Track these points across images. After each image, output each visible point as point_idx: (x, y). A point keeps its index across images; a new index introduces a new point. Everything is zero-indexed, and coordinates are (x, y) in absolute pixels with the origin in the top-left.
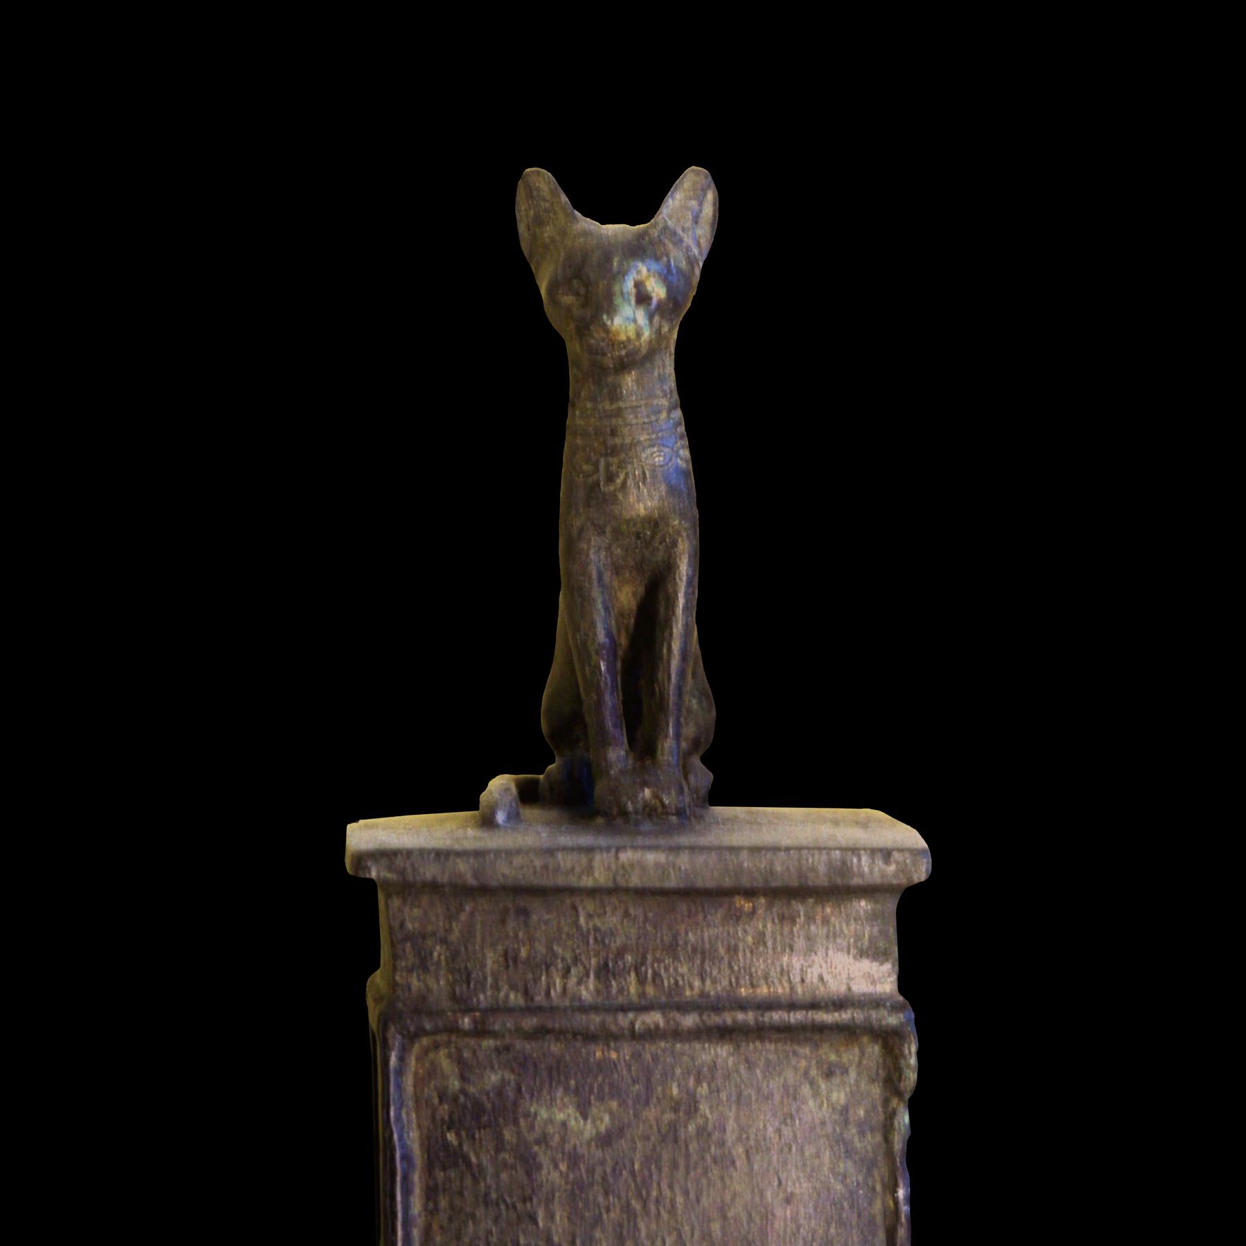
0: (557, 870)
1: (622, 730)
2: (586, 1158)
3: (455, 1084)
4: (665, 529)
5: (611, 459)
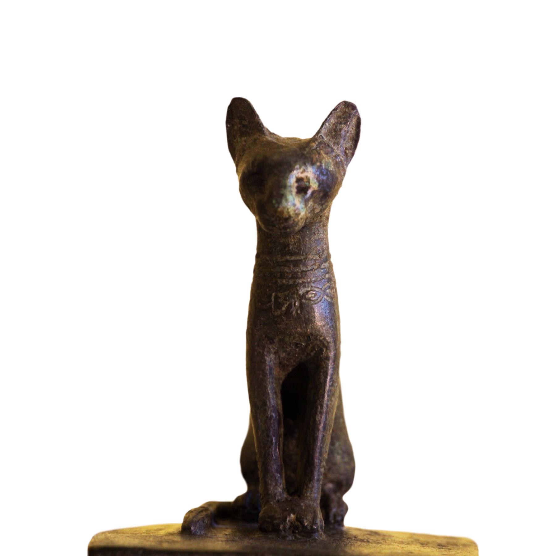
1: (330, 461)
5: (279, 294)
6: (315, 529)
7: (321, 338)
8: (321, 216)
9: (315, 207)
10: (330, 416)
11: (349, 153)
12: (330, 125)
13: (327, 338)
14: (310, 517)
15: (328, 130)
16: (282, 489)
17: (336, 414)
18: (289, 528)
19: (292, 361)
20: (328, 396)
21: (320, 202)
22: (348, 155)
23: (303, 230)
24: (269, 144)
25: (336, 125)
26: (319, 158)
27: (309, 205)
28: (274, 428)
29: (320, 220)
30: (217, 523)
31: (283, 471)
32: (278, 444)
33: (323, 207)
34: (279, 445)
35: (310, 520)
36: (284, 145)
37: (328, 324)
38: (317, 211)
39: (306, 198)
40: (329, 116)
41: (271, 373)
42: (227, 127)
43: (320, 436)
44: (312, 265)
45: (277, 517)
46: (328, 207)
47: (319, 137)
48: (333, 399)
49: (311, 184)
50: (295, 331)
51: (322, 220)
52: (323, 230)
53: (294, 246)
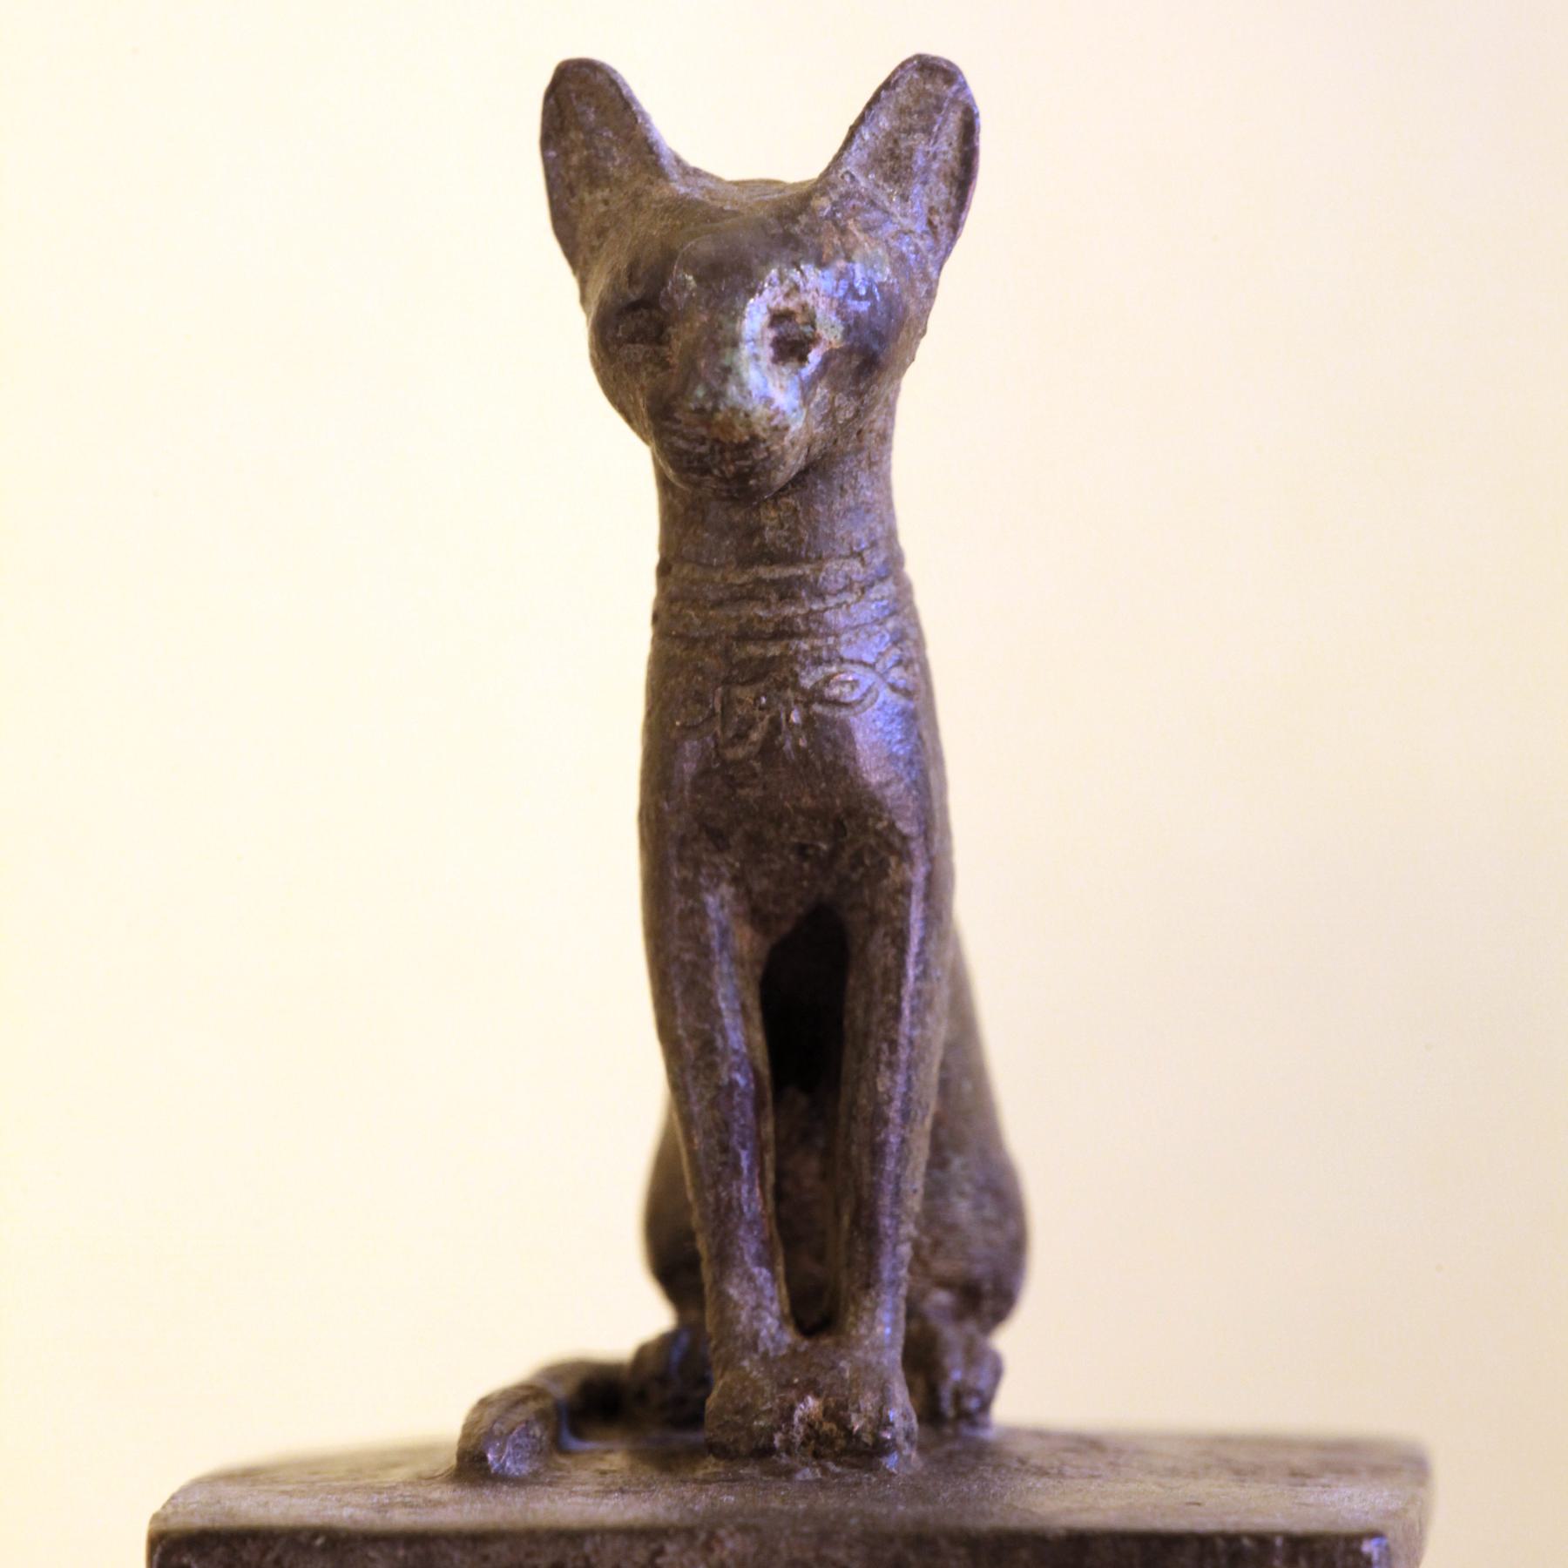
6: (886, 1441)
7: (880, 826)
8: (859, 432)
9: (836, 404)
10: (922, 1076)
11: (942, 223)
12: (877, 138)
13: (900, 825)
14: (868, 1402)
15: (869, 155)
16: (779, 1319)
17: (944, 1066)
18: (803, 1444)
19: (792, 903)
20: (913, 1011)
21: (853, 388)
22: (939, 229)
23: (804, 480)
24: (682, 209)
25: (896, 135)
26: (843, 244)
27: (818, 399)
28: (742, 1122)
29: (857, 443)
30: (578, 1433)
31: (780, 1259)
32: (757, 1171)
33: (862, 402)
34: (762, 1176)
35: (868, 1414)
36: (728, 207)
37: (901, 779)
38: (845, 415)
39: (803, 377)
40: (869, 106)
41: (723, 946)
42: (545, 159)
43: (894, 1139)
44: (840, 591)
45: (764, 1408)
46: (883, 400)
47: (842, 177)
48: (929, 1019)
49: (820, 331)
50: (794, 807)
51: (866, 443)
52: (870, 475)
53: (779, 532)
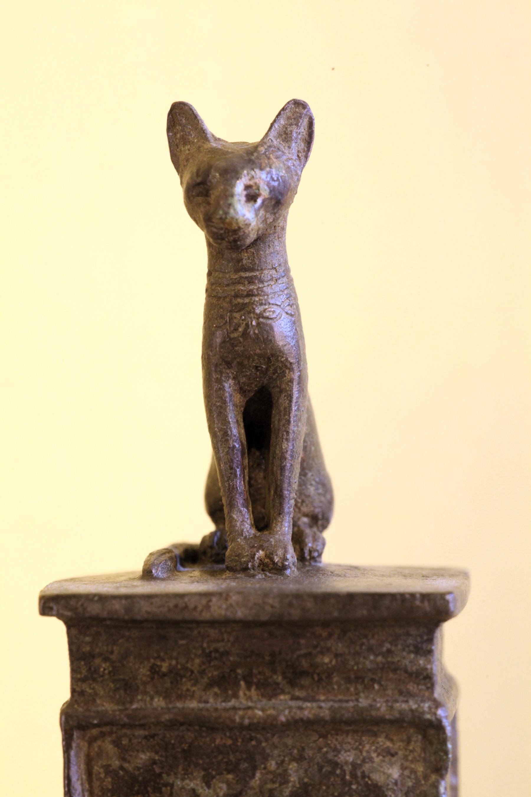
0: (186, 607)
2: (336, 705)
3: (116, 763)
4: (277, 364)
